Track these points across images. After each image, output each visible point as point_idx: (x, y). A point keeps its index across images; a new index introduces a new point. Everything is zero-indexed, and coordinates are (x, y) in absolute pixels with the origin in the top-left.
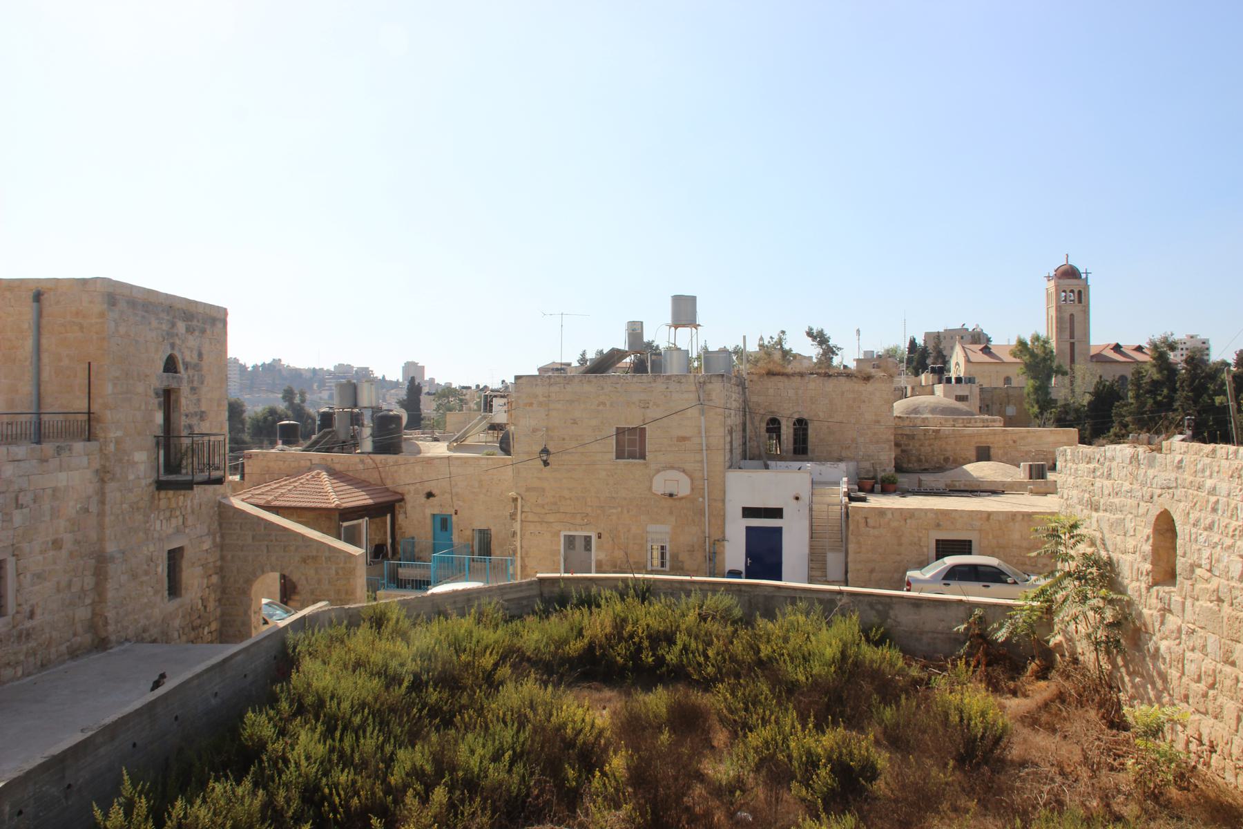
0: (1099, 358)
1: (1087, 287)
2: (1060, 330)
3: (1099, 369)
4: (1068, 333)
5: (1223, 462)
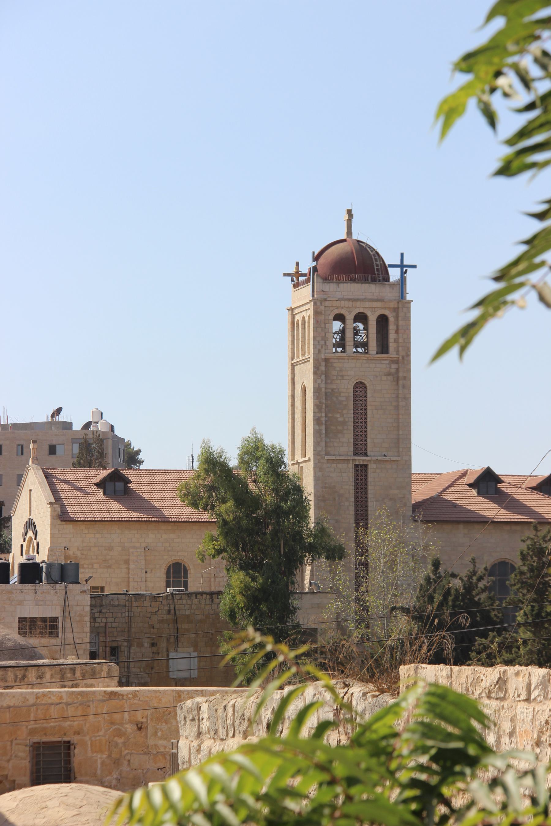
0: (437, 513)
1: (402, 305)
2: (326, 429)
3: (432, 542)
4: (348, 437)
5: (522, 707)
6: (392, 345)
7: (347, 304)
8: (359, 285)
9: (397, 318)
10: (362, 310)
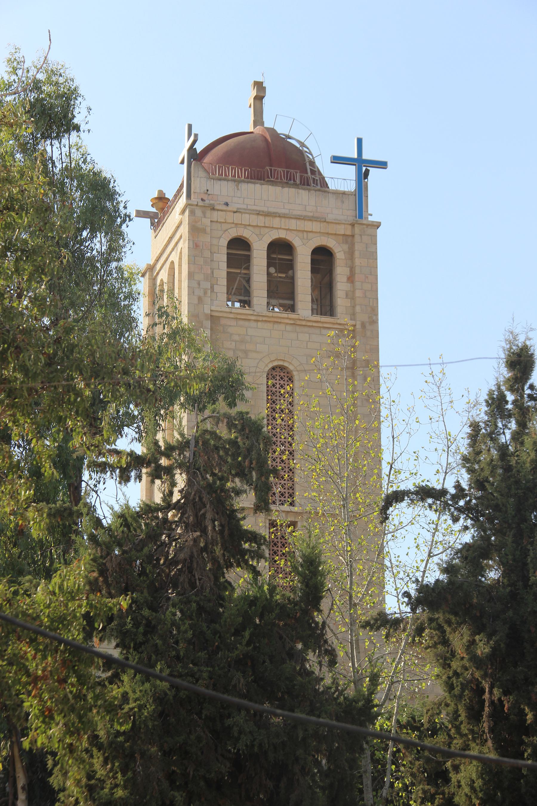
1: (361, 228)
6: (341, 301)
7: (255, 220)
8: (278, 189)
9: (351, 254)
10: (282, 235)
